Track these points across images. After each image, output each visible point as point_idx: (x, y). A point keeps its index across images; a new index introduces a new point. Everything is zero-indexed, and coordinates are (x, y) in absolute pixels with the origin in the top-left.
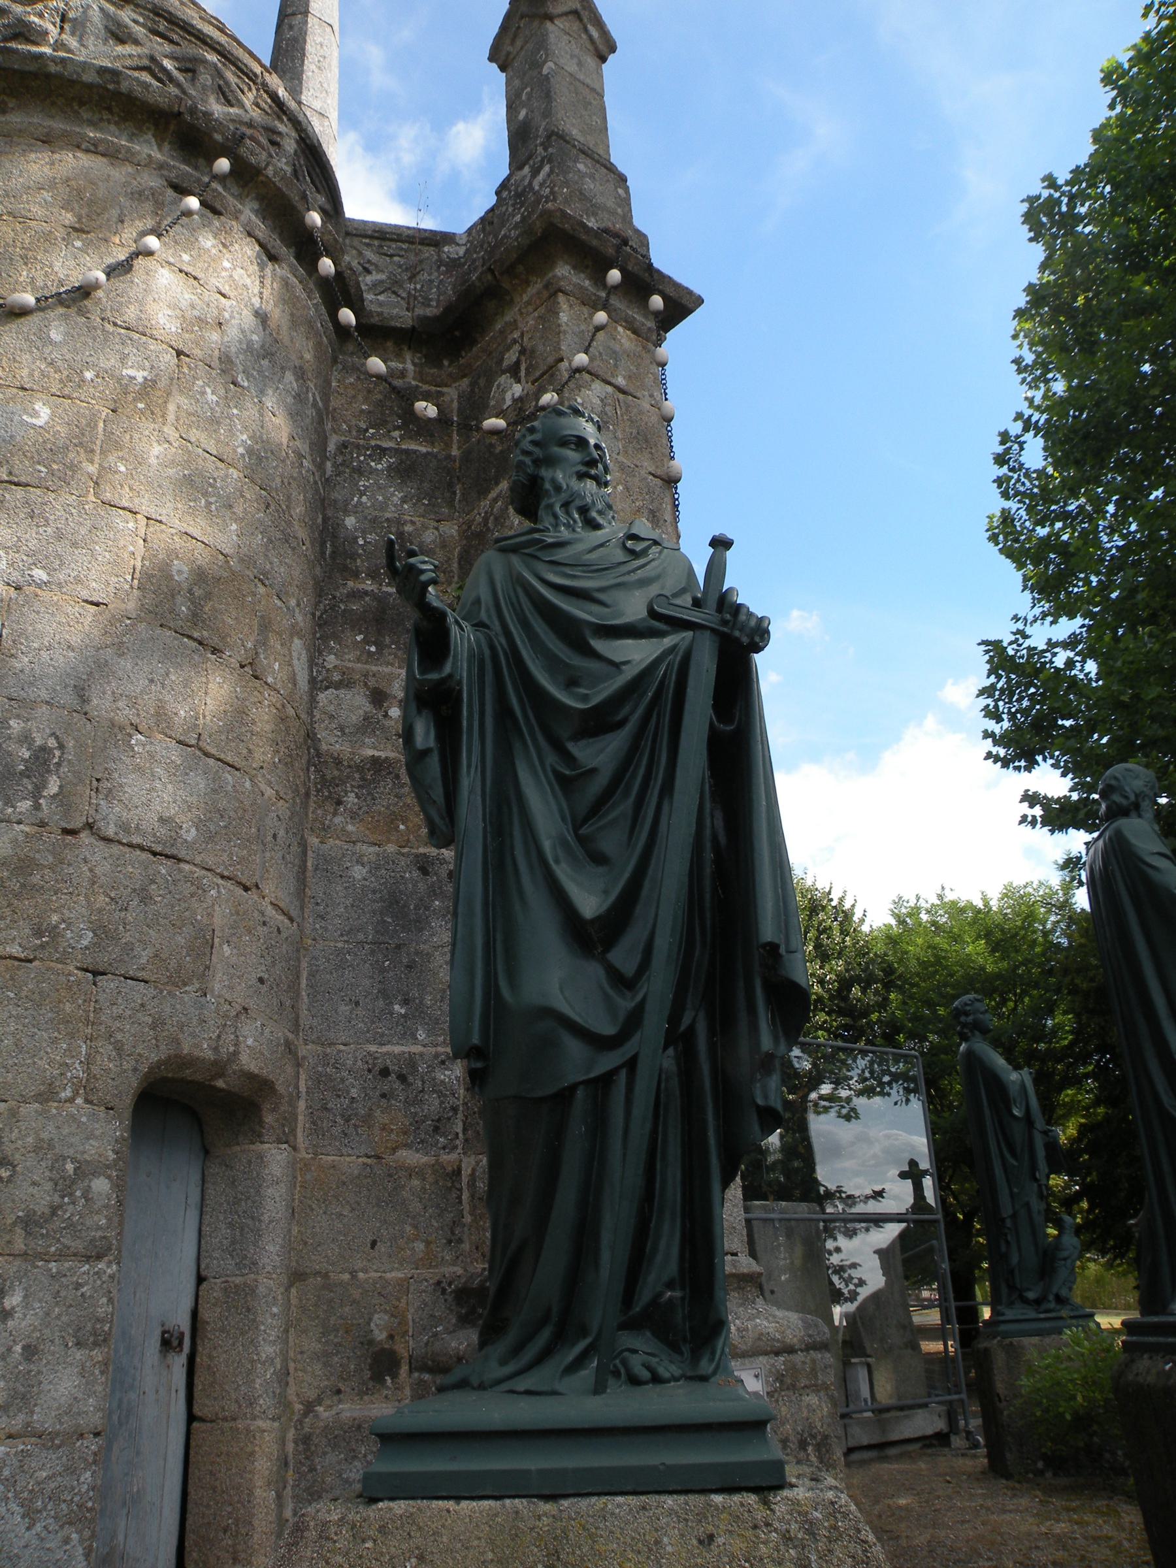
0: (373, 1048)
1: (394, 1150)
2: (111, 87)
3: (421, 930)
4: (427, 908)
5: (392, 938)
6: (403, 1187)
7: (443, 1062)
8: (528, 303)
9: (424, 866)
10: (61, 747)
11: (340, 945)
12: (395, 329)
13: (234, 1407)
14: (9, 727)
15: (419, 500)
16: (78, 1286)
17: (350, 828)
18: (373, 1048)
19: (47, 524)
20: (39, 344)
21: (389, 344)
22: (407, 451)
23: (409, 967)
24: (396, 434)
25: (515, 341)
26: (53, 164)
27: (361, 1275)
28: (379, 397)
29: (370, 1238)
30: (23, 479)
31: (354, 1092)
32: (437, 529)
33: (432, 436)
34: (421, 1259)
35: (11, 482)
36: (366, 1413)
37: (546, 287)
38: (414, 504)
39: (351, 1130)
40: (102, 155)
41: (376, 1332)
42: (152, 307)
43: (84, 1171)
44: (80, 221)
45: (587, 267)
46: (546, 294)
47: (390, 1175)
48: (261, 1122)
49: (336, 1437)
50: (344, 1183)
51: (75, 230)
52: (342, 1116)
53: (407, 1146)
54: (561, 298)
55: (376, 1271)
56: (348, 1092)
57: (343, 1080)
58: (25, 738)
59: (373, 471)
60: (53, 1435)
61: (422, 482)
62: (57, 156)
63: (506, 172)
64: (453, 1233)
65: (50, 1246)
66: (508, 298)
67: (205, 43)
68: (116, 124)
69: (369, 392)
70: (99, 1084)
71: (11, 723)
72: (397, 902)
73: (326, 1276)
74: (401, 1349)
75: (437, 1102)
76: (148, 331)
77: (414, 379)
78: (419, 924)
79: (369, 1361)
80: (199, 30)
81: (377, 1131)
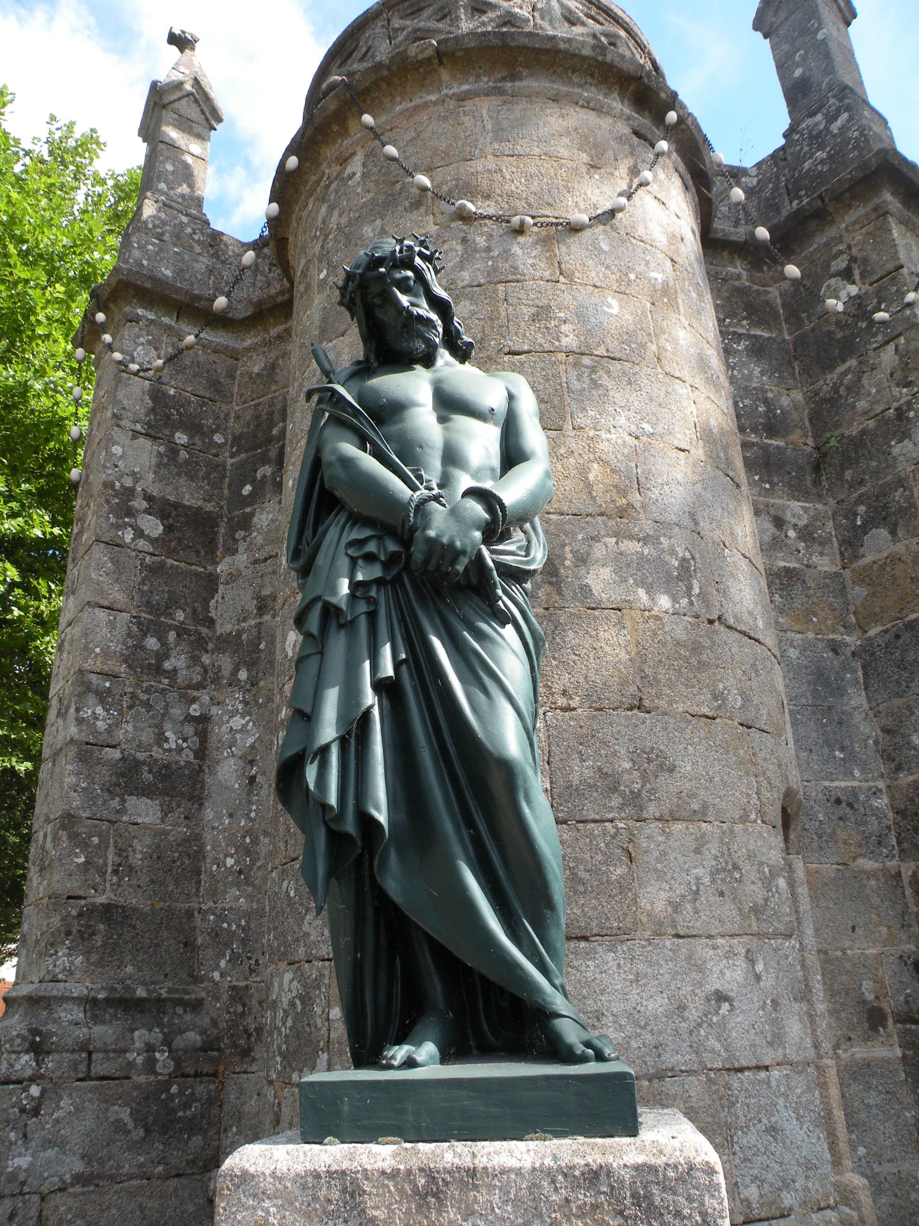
0: (827, 784)
1: (855, 858)
2: (600, 58)
3: (842, 695)
4: (843, 680)
5: (824, 702)
6: (865, 886)
7: (875, 793)
8: (855, 222)
9: (835, 648)
12: (733, 242)
14: (661, 543)
15: (772, 374)
18: (827, 784)
19: (641, 390)
20: (596, 252)
21: (725, 254)
22: (755, 336)
23: (840, 723)
24: (745, 322)
25: (841, 252)
26: (563, 117)
27: (849, 952)
28: (726, 294)
29: (850, 925)
30: (617, 355)
31: (821, 817)
32: (788, 395)
33: (769, 324)
34: (886, 940)
35: (609, 357)
36: (871, 1055)
37: (875, 209)
38: (770, 377)
39: (824, 845)
40: (593, 110)
41: (867, 994)
42: (651, 225)
44: (592, 160)
45: (899, 194)
46: (874, 215)
47: (855, 877)
49: (854, 1072)
50: (826, 884)
51: (592, 166)
52: (816, 833)
53: (863, 856)
54: (890, 219)
55: (859, 949)
56: (817, 816)
57: (812, 808)
59: (736, 351)
60: (798, 1063)
61: (771, 360)
62: (564, 111)
63: (785, 122)
64: (904, 920)
65: (769, 928)
66: (829, 218)
67: (618, 23)
68: (595, 86)
69: (719, 290)
71: (662, 539)
72: (823, 675)
74: (886, 1006)
75: (876, 822)
76: (654, 244)
77: (747, 280)
78: (840, 692)
79: (866, 1016)
80: (615, 14)
81: (841, 845)
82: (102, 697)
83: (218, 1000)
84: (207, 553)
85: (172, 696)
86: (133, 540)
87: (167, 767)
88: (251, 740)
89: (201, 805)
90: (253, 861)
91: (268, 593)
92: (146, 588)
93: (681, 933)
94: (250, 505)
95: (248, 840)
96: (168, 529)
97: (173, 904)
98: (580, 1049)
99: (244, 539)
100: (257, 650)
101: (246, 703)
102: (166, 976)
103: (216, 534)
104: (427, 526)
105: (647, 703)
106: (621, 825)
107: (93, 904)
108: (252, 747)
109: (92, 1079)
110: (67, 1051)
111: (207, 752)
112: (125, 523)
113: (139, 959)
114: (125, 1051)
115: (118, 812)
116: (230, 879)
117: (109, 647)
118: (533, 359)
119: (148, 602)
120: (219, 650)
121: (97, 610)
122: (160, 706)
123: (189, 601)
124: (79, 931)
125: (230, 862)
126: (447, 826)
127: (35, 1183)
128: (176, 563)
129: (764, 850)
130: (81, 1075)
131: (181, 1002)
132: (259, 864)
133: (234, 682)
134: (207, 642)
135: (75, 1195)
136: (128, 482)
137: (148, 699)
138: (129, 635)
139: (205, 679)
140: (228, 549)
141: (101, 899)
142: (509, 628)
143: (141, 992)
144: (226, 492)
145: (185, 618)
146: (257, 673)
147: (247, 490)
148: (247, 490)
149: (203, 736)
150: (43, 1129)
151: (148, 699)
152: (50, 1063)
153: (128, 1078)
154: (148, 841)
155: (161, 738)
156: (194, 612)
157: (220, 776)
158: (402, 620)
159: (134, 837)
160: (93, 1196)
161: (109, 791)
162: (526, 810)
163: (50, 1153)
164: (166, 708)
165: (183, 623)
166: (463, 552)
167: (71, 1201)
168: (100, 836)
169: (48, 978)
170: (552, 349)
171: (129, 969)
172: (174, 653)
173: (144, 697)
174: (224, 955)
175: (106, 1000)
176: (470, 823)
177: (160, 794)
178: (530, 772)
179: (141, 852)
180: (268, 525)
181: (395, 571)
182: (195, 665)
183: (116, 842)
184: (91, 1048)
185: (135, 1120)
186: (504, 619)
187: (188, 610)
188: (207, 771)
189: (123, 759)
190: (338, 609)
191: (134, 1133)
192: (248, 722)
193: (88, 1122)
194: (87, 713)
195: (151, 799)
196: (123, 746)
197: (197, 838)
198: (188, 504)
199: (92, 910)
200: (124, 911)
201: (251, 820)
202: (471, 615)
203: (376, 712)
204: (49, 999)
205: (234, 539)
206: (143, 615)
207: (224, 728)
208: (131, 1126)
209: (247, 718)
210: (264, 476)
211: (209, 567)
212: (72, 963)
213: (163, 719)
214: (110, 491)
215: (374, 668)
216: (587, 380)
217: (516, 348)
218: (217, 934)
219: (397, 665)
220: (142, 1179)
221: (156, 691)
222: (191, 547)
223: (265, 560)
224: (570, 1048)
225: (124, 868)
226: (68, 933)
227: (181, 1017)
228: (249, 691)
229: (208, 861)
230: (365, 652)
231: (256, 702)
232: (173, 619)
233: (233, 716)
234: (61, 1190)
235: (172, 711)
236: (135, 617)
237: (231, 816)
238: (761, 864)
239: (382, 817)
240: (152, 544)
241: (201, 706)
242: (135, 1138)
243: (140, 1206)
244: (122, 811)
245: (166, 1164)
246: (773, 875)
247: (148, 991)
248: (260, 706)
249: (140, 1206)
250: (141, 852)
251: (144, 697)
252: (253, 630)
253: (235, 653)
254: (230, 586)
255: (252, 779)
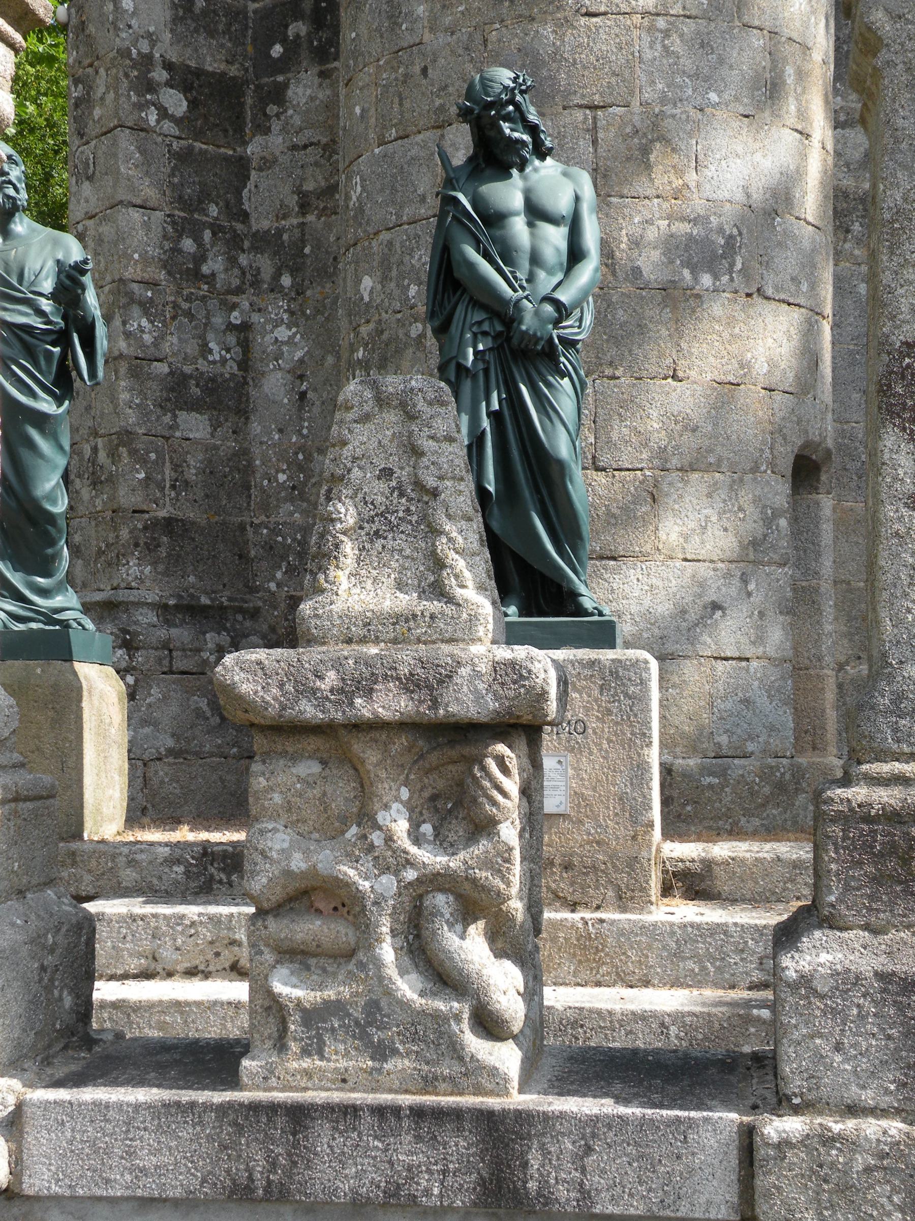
10: (740, 234)
11: (851, 347)
13: (807, 662)
16: (778, 580)
17: (856, 252)
35: (685, 16)
43: (776, 514)
48: (818, 480)
57: (856, 449)
58: (721, 230)
70: (778, 462)
73: (849, 583)
82: (146, 307)
83: (275, 608)
84: (235, 131)
85: (213, 304)
86: (158, 121)
87: (213, 380)
88: (299, 354)
89: (247, 418)
90: (308, 478)
91: (311, 189)
92: (176, 180)
93: (689, 558)
94: (281, 71)
95: (301, 456)
96: (193, 104)
97: (227, 518)
98: (590, 610)
99: (278, 116)
100: (300, 254)
101: (292, 313)
102: (224, 585)
103: (242, 105)
104: (520, 322)
105: (680, 374)
106: (648, 473)
107: (156, 518)
108: (301, 361)
109: (172, 673)
110: (152, 648)
111: (250, 363)
112: (147, 101)
113: (200, 569)
114: (199, 650)
115: (171, 427)
116: (283, 494)
117: (147, 252)
118: (609, 23)
119: (180, 197)
120: (255, 249)
121: (131, 210)
122: (201, 315)
123: (222, 192)
124: (146, 543)
125: (282, 477)
126: (527, 493)
127: (138, 752)
128: (204, 147)
129: (770, 496)
130: (165, 669)
131: (240, 610)
132: (313, 480)
133: (276, 287)
134: (242, 241)
135: (170, 764)
136: (145, 47)
137: (190, 309)
138: (165, 237)
139: (243, 283)
140: (259, 126)
141: (162, 514)
142: (566, 379)
143: (205, 600)
144: (250, 49)
145: (219, 213)
146: (303, 281)
147: (277, 50)
148: (277, 50)
149: (245, 345)
150: (140, 711)
151: (190, 309)
152: (140, 657)
153: (203, 674)
154: (200, 457)
155: (205, 350)
156: (227, 205)
157: (266, 389)
158: (503, 371)
159: (188, 453)
160: (183, 767)
161: (161, 407)
162: (570, 487)
163: (147, 730)
164: (207, 317)
165: (217, 219)
166: (541, 338)
167: (166, 768)
168: (156, 452)
169: (123, 585)
170: (628, 10)
171: (192, 579)
172: (210, 255)
173: (185, 306)
174: (280, 567)
175: (176, 606)
176: (538, 491)
177: (208, 409)
178: (573, 465)
179: (195, 467)
180: (306, 103)
181: (499, 342)
182: (233, 267)
183: (171, 458)
184: (171, 646)
185: (212, 710)
186: (563, 375)
187: (221, 204)
188: (251, 383)
189: (171, 373)
190: (467, 369)
191: (212, 720)
192: (295, 334)
193: (174, 708)
194: (133, 326)
195: (201, 413)
196: (170, 360)
197: (245, 452)
198: (210, 69)
199: (156, 522)
200: (184, 525)
201: (303, 436)
202: (544, 371)
203: (488, 429)
204: (127, 603)
205: (265, 114)
206: (177, 212)
207: (268, 338)
208: (209, 714)
209: (294, 330)
210: (298, 36)
211: (238, 149)
212: (142, 572)
213: (205, 328)
214: (128, 62)
215: (488, 405)
216: (658, 46)
217: (593, 9)
218: (271, 548)
219: (500, 402)
220: (220, 757)
221: (197, 299)
222: (217, 125)
223: (305, 147)
224: (586, 610)
225: (180, 484)
226: (137, 545)
227: (241, 623)
228: (294, 299)
229: (258, 475)
230: (482, 395)
231: (304, 313)
232: (207, 215)
233: (277, 326)
234: (159, 759)
235: (213, 320)
236: (169, 216)
237: (281, 431)
238: (765, 507)
239: (491, 488)
240: (177, 125)
241: (241, 313)
242: (213, 724)
243: (221, 778)
244: (174, 427)
245: (239, 747)
246: (776, 514)
247: (211, 599)
248: (308, 318)
249: (221, 778)
250: (195, 467)
251: (185, 306)
252: (296, 231)
253: (275, 255)
254: (264, 173)
255: (303, 395)
